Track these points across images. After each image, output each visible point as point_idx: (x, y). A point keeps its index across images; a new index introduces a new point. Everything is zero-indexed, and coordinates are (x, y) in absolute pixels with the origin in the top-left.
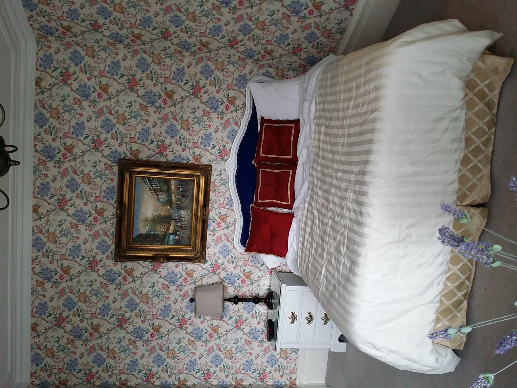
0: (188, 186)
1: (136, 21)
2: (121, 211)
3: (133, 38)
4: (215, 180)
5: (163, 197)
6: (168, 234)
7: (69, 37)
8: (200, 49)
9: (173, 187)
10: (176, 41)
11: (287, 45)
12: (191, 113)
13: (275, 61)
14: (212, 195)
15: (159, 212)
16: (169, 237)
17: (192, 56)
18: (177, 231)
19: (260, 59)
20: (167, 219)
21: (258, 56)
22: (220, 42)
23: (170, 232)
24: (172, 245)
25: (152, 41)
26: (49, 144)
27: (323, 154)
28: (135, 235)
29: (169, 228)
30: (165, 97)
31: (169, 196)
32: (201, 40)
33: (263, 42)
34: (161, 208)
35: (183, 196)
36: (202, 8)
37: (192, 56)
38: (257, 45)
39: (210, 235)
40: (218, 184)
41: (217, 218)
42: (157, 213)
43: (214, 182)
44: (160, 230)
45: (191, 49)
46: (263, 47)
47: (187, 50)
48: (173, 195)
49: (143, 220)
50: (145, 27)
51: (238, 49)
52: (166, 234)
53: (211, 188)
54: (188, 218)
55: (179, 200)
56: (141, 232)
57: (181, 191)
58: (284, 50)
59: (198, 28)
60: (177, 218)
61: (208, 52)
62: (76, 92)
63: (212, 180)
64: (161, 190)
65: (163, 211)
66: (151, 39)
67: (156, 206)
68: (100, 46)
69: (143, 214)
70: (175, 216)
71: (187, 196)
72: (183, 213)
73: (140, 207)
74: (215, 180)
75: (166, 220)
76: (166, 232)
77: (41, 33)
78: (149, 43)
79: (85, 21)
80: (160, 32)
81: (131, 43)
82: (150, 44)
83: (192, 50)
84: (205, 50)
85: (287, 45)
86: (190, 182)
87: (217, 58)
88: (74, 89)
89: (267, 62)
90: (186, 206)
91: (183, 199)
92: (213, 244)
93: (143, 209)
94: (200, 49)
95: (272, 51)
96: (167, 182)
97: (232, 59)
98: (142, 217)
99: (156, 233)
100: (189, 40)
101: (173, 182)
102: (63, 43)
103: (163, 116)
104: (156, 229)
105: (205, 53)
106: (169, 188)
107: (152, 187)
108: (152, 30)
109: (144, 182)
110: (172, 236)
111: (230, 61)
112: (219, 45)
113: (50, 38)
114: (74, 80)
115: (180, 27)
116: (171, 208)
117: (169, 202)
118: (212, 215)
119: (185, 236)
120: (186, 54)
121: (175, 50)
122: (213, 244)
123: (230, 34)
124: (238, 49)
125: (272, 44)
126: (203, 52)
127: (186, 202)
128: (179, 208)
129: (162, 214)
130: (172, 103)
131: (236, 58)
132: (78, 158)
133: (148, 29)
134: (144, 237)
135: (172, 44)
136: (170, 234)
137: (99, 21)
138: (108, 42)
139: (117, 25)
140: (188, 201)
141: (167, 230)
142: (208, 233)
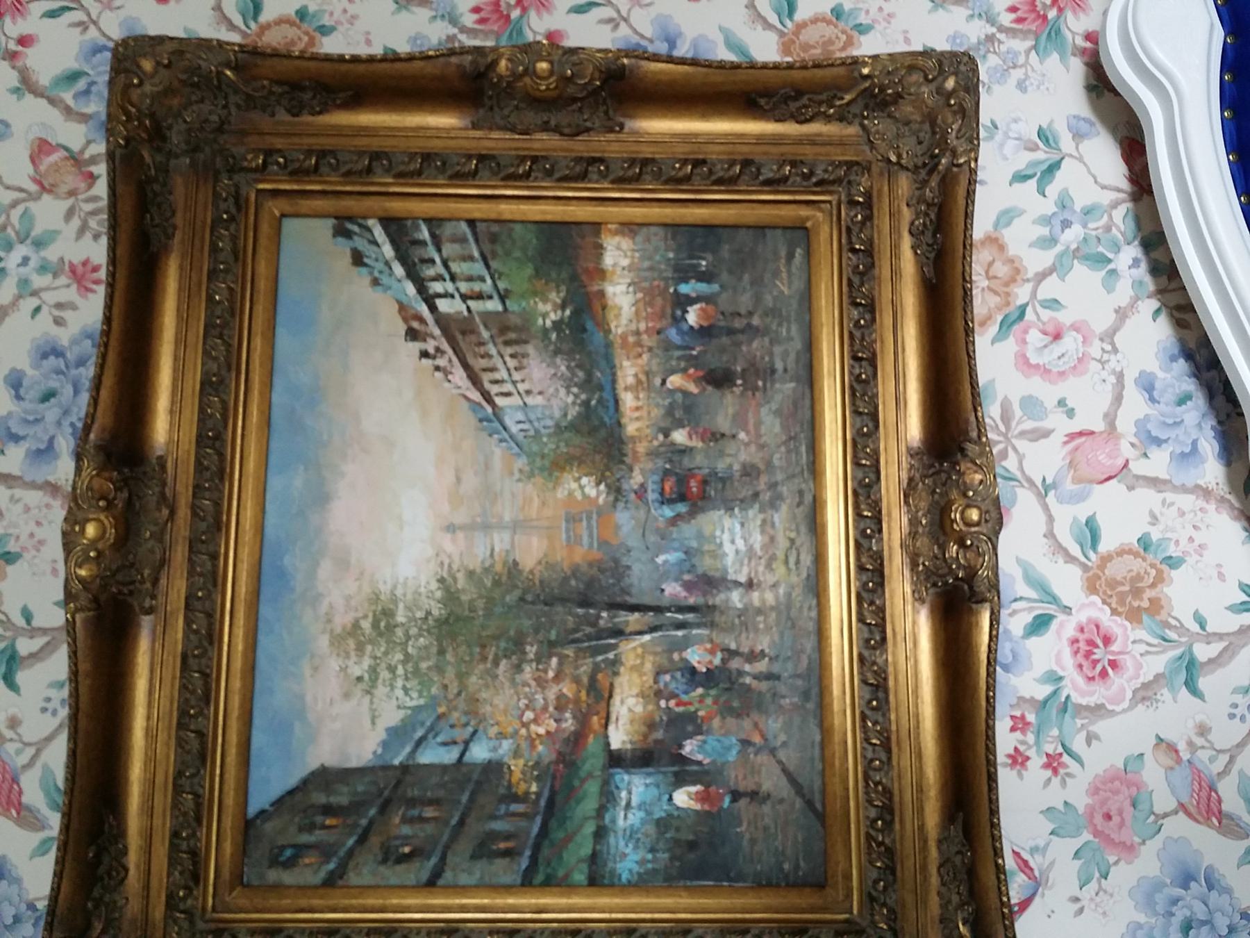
0: (757, 282)
2: (128, 526)
4: (1007, 217)
5: (539, 389)
6: (592, 760)
9: (621, 298)
12: (1020, 177)
14: (994, 361)
15: (501, 541)
16: (608, 797)
18: (684, 724)
20: (576, 610)
23: (618, 738)
24: (641, 884)
28: (271, 781)
29: (599, 696)
30: (1093, 610)
31: (589, 384)
34: (519, 495)
35: (719, 379)
39: (1019, 759)
40: (1036, 261)
41: (1067, 582)
42: (480, 551)
43: (994, 241)
44: (514, 719)
48: (628, 371)
49: (342, 620)
52: (568, 772)
53: (982, 303)
54: (778, 585)
55: (682, 411)
56: (325, 752)
57: (705, 332)
60: (673, 589)
62: (52, 101)
63: (981, 226)
64: (512, 332)
65: (542, 524)
67: (471, 482)
69: (343, 563)
70: (655, 570)
71: (758, 376)
72: (733, 539)
73: (321, 497)
74: (1007, 217)
75: (567, 616)
76: (577, 739)
86: (778, 241)
88: (44, 79)
90: (749, 472)
91: (724, 409)
92: (1061, 861)
93: (345, 515)
96: (564, 254)
98: (338, 597)
99: (480, 752)
101: (617, 254)
103: (1094, 790)
104: (473, 709)
106: (585, 309)
107: (430, 301)
109: (358, 259)
110: (636, 788)
114: (52, 14)
116: (617, 491)
117: (595, 438)
118: (1023, 550)
119: (771, 780)
122: (1061, 861)
127: (751, 430)
128: (690, 491)
129: (531, 553)
130: (1157, 664)
132: (34, 657)
134: (357, 806)
136: (616, 760)
140: (772, 427)
141: (583, 721)
142: (1005, 740)
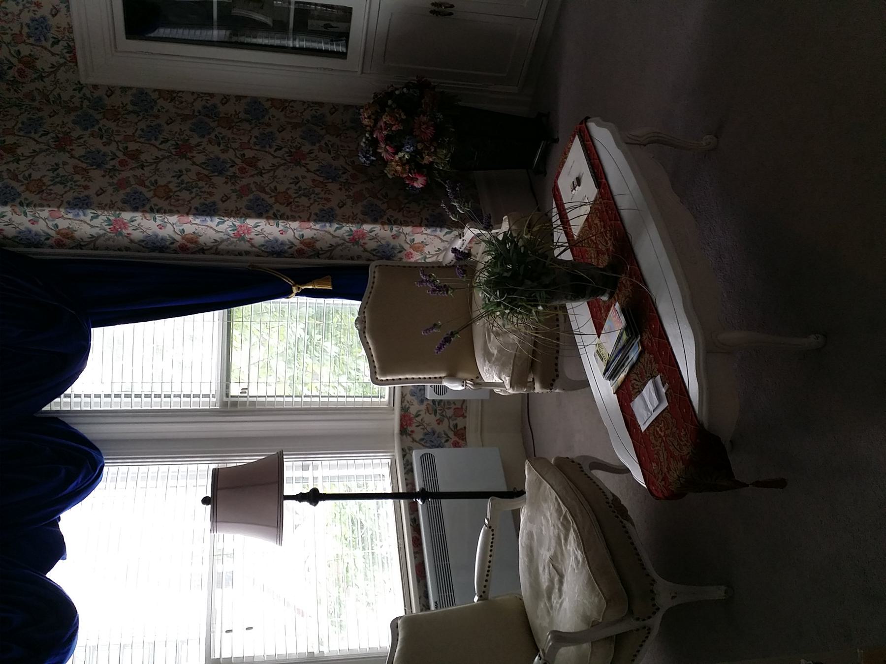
1: (137, 130)
3: (125, 158)
7: (131, 169)
8: (123, 163)
10: (200, 158)
11: (42, 135)
13: (22, 164)
17: (107, 177)
19: (118, 167)
21: (112, 163)
22: (38, 142)
25: (158, 160)
26: (432, 429)
27: (477, 381)
32: (127, 147)
33: (234, 145)
36: (82, 92)
37: (107, 177)
38: (109, 144)
45: (228, 170)
46: (121, 146)
47: (220, 173)
50: (264, 147)
51: (195, 159)
58: (275, 157)
59: (122, 130)
61: (257, 174)
66: (274, 165)
68: (182, 182)
77: (317, 178)
78: (151, 164)
79: (167, 141)
80: (173, 145)
81: (351, 181)
82: (271, 174)
83: (228, 173)
84: (133, 164)
85: (42, 135)
87: (274, 184)
89: (5, 167)
94: (242, 170)
95: (16, 145)
97: (61, 171)
100: (223, 156)
102: (351, 194)
105: (252, 176)
108: (275, 151)
111: (182, 182)
112: (159, 154)
113: (330, 186)
115: (318, 145)
120: (218, 180)
121: (314, 181)
123: (177, 135)
124: (73, 152)
125: (14, 135)
126: (129, 167)
131: (69, 169)
133: (267, 149)
135: (194, 163)
137: (303, 148)
138: (314, 181)
139: (330, 153)
